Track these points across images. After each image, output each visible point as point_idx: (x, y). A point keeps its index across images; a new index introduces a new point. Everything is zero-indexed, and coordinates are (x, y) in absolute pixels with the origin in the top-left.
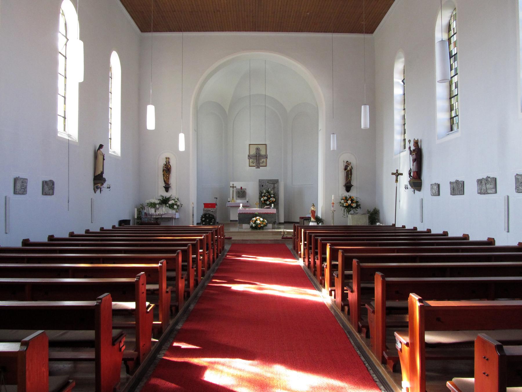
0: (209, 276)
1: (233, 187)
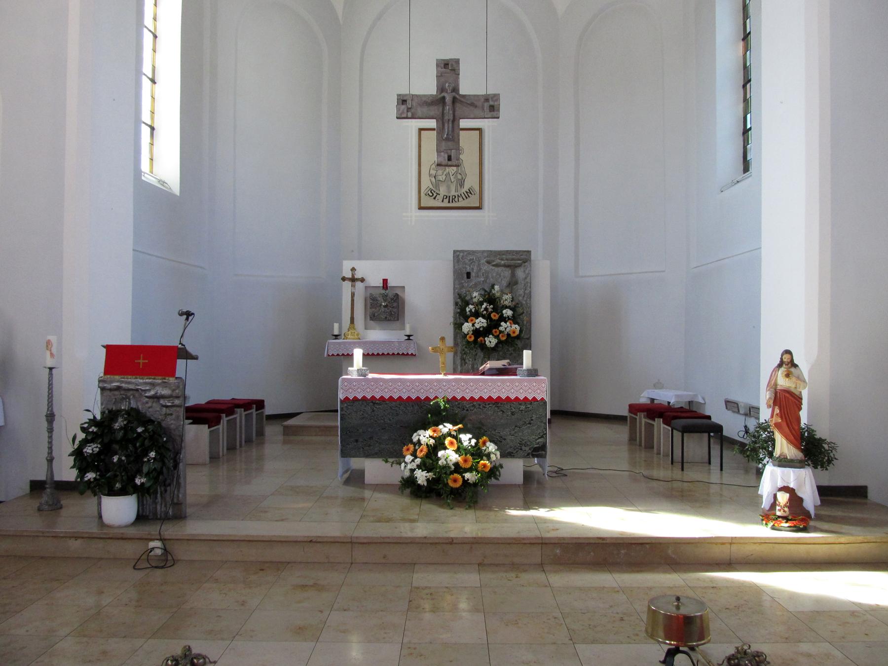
1: (353, 280)
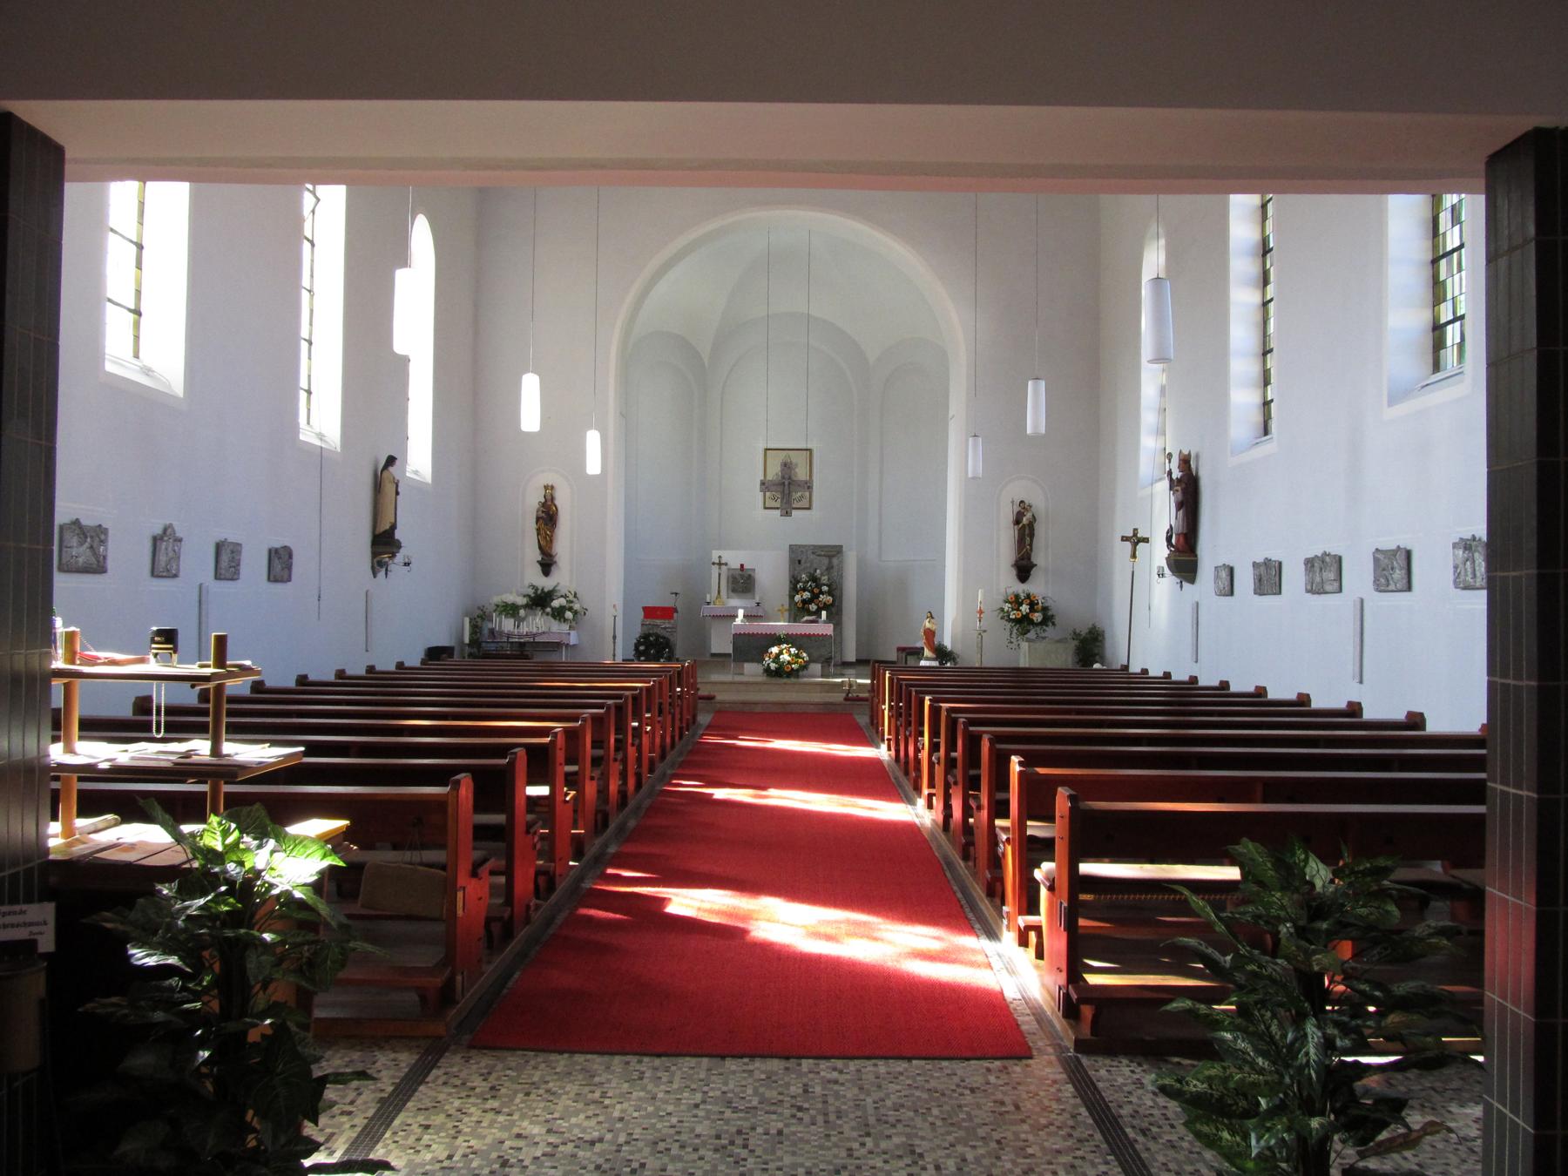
0: (664, 774)
